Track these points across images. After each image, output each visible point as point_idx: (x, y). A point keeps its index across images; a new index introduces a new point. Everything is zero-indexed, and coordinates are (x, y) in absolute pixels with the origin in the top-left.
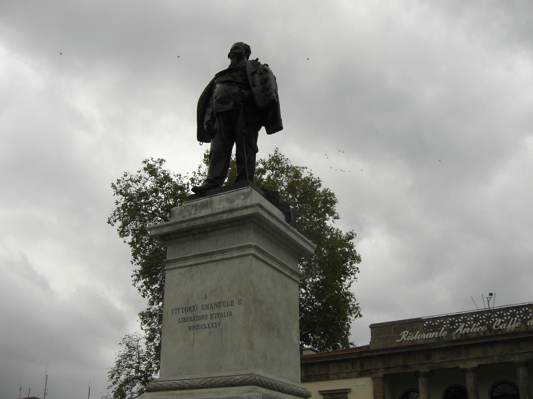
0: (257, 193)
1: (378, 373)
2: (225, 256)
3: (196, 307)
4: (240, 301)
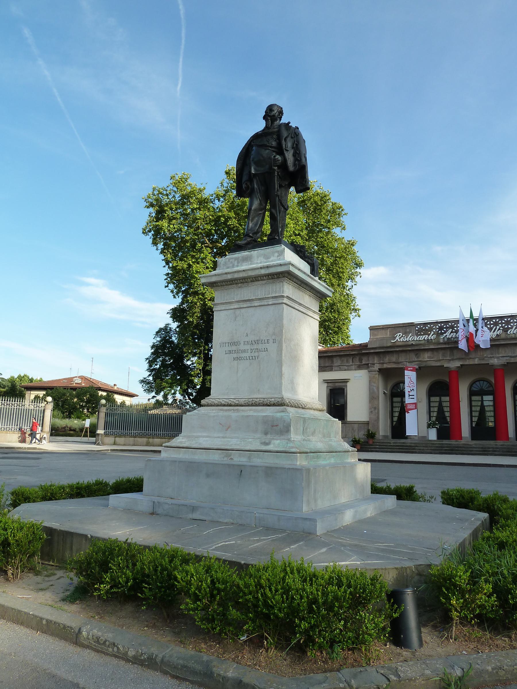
1: (374, 367)
2: (262, 303)
3: (239, 343)
4: (274, 340)
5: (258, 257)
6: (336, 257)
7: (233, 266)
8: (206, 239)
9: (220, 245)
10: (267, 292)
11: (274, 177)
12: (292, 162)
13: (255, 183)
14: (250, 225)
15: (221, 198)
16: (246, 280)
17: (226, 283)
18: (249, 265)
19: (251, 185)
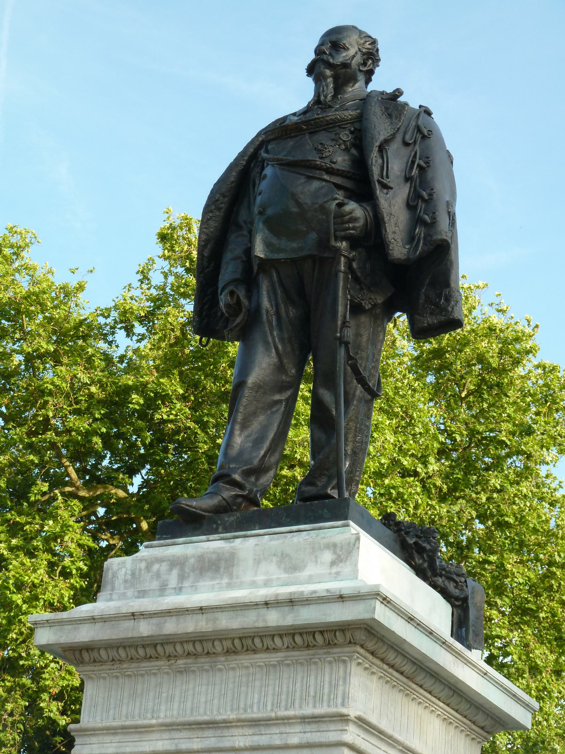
0: (407, 191)
5: (258, 562)
6: (551, 563)
7: (163, 589)
8: (71, 470)
9: (121, 493)
10: (284, 697)
11: (336, 275)
12: (401, 226)
13: (264, 293)
14: (238, 440)
15: (136, 324)
16: (208, 646)
17: (132, 652)
18: (221, 589)
19: (249, 297)
